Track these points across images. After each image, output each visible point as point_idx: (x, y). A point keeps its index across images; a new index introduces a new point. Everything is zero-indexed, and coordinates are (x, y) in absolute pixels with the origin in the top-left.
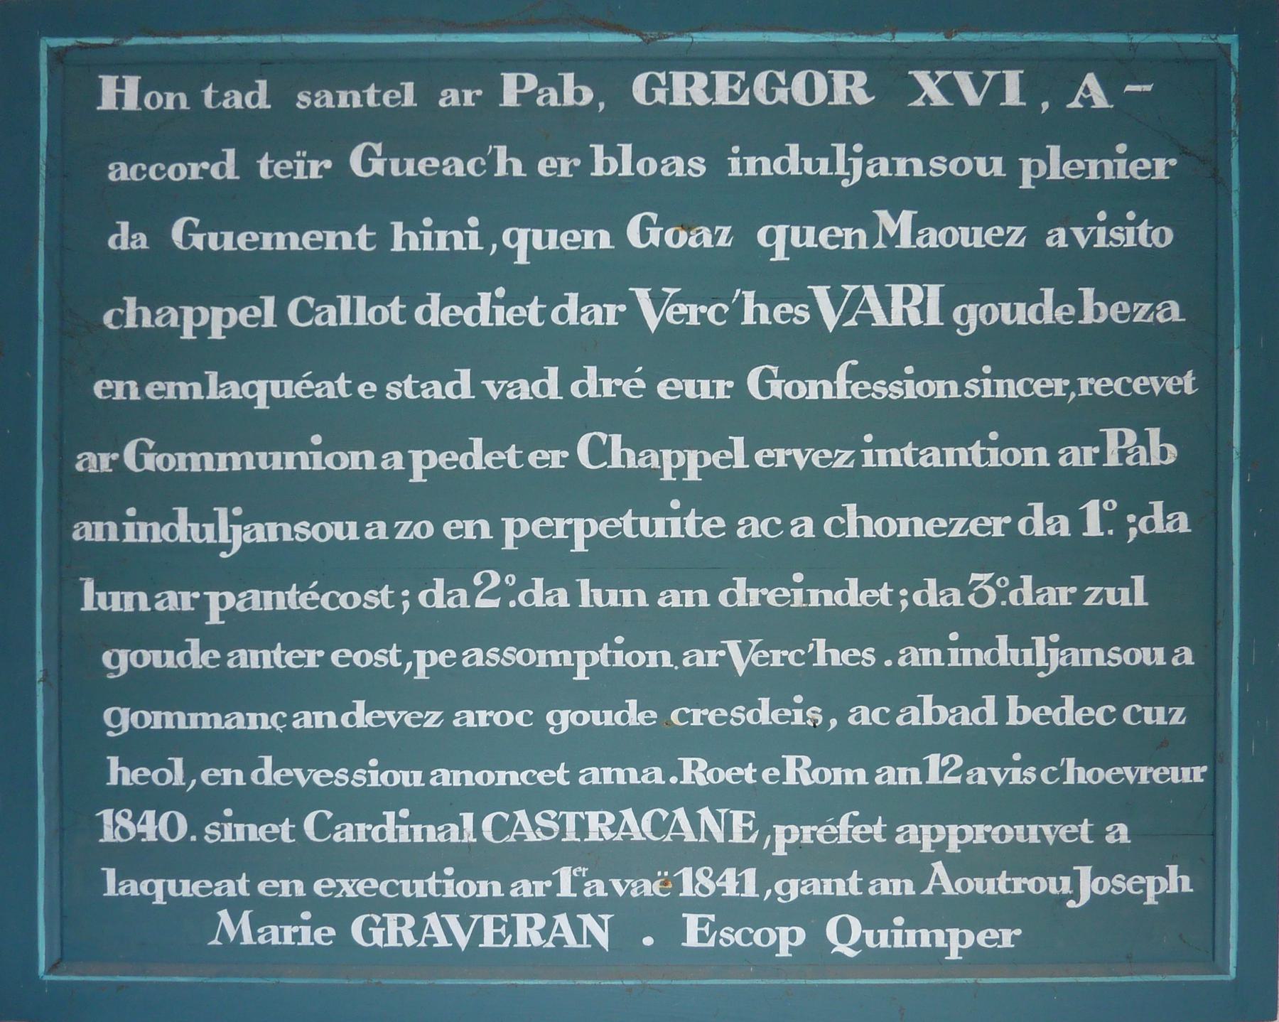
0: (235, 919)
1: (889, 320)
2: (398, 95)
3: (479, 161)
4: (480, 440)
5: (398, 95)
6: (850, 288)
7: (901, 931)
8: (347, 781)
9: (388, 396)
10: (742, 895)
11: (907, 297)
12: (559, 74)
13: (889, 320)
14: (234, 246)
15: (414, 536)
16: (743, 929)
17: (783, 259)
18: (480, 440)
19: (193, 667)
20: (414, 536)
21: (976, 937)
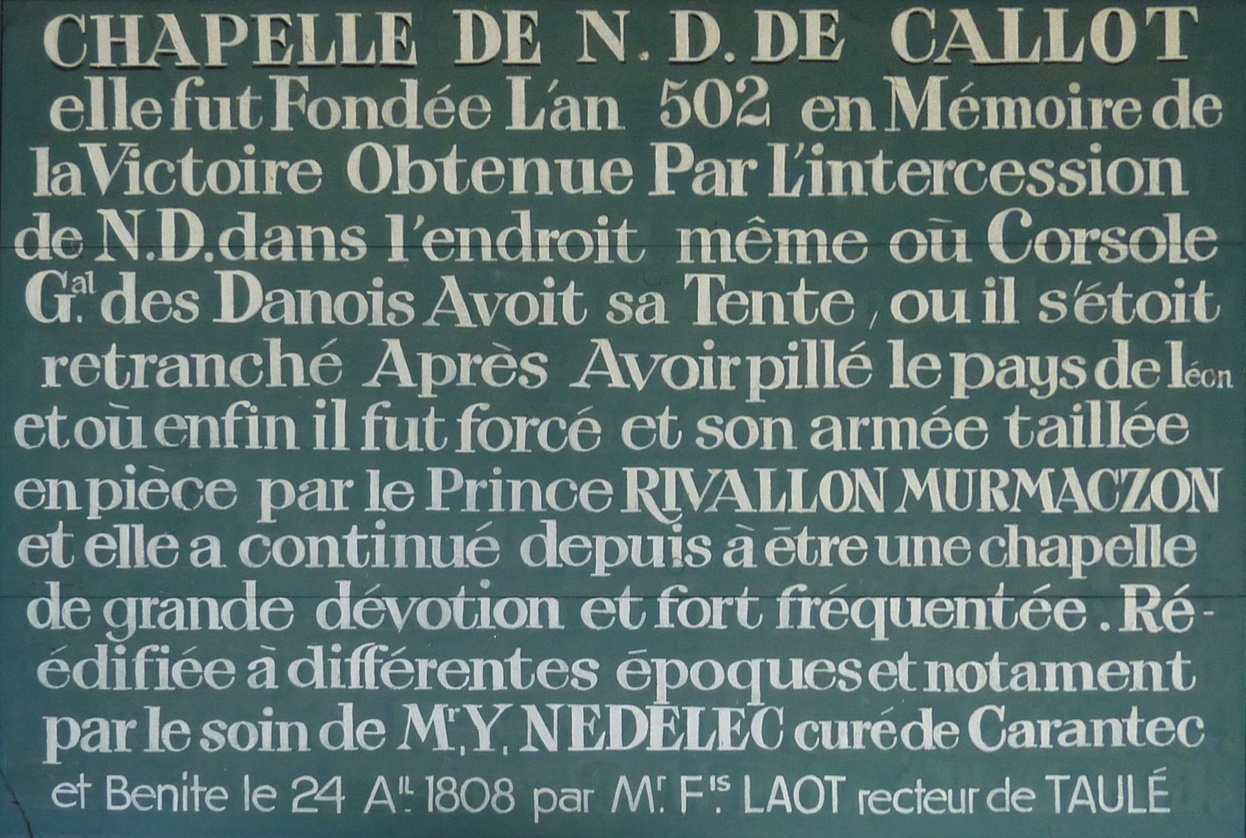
0: (918, 90)
1: (677, 475)
2: (79, 106)
3: (1194, 722)
4: (343, 402)
5: (79, 106)
6: (714, 473)
7: (607, 231)
8: (1063, 167)
9: (195, 296)
10: (763, 660)
11: (643, 480)
12: (239, 213)
13: (677, 475)
14: (1094, 686)
15: (1152, 504)
16: (683, 387)
17: (280, 385)
18: (343, 402)
19: (410, 450)
20: (1152, 504)
21: (634, 315)
